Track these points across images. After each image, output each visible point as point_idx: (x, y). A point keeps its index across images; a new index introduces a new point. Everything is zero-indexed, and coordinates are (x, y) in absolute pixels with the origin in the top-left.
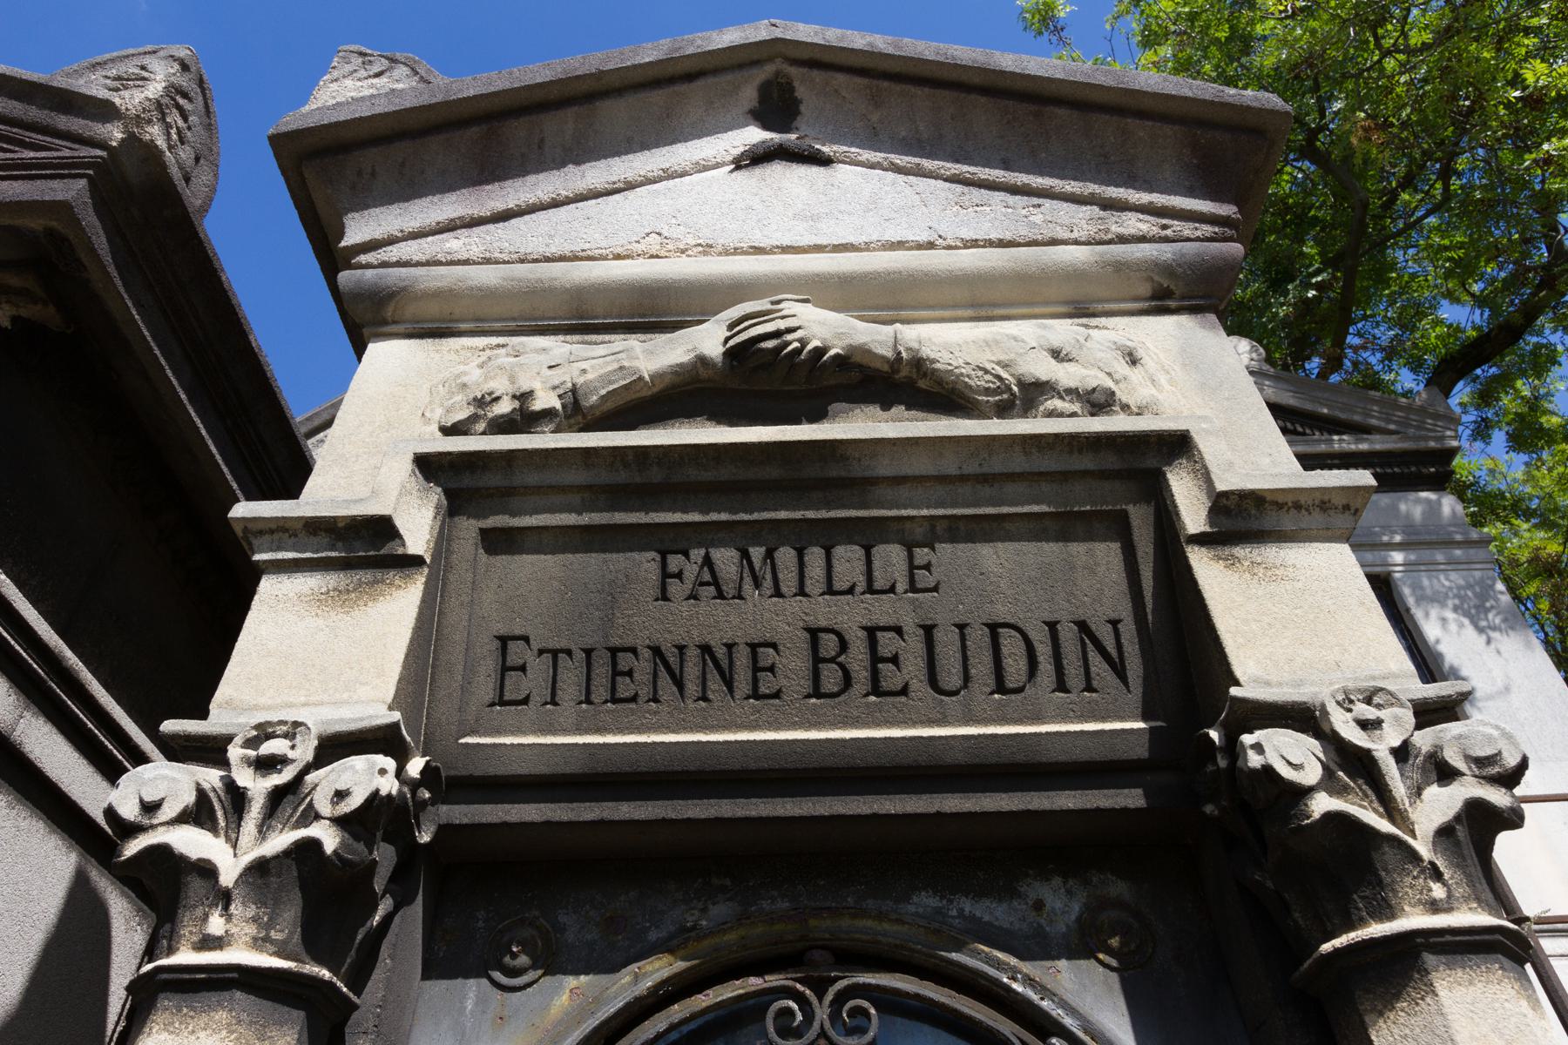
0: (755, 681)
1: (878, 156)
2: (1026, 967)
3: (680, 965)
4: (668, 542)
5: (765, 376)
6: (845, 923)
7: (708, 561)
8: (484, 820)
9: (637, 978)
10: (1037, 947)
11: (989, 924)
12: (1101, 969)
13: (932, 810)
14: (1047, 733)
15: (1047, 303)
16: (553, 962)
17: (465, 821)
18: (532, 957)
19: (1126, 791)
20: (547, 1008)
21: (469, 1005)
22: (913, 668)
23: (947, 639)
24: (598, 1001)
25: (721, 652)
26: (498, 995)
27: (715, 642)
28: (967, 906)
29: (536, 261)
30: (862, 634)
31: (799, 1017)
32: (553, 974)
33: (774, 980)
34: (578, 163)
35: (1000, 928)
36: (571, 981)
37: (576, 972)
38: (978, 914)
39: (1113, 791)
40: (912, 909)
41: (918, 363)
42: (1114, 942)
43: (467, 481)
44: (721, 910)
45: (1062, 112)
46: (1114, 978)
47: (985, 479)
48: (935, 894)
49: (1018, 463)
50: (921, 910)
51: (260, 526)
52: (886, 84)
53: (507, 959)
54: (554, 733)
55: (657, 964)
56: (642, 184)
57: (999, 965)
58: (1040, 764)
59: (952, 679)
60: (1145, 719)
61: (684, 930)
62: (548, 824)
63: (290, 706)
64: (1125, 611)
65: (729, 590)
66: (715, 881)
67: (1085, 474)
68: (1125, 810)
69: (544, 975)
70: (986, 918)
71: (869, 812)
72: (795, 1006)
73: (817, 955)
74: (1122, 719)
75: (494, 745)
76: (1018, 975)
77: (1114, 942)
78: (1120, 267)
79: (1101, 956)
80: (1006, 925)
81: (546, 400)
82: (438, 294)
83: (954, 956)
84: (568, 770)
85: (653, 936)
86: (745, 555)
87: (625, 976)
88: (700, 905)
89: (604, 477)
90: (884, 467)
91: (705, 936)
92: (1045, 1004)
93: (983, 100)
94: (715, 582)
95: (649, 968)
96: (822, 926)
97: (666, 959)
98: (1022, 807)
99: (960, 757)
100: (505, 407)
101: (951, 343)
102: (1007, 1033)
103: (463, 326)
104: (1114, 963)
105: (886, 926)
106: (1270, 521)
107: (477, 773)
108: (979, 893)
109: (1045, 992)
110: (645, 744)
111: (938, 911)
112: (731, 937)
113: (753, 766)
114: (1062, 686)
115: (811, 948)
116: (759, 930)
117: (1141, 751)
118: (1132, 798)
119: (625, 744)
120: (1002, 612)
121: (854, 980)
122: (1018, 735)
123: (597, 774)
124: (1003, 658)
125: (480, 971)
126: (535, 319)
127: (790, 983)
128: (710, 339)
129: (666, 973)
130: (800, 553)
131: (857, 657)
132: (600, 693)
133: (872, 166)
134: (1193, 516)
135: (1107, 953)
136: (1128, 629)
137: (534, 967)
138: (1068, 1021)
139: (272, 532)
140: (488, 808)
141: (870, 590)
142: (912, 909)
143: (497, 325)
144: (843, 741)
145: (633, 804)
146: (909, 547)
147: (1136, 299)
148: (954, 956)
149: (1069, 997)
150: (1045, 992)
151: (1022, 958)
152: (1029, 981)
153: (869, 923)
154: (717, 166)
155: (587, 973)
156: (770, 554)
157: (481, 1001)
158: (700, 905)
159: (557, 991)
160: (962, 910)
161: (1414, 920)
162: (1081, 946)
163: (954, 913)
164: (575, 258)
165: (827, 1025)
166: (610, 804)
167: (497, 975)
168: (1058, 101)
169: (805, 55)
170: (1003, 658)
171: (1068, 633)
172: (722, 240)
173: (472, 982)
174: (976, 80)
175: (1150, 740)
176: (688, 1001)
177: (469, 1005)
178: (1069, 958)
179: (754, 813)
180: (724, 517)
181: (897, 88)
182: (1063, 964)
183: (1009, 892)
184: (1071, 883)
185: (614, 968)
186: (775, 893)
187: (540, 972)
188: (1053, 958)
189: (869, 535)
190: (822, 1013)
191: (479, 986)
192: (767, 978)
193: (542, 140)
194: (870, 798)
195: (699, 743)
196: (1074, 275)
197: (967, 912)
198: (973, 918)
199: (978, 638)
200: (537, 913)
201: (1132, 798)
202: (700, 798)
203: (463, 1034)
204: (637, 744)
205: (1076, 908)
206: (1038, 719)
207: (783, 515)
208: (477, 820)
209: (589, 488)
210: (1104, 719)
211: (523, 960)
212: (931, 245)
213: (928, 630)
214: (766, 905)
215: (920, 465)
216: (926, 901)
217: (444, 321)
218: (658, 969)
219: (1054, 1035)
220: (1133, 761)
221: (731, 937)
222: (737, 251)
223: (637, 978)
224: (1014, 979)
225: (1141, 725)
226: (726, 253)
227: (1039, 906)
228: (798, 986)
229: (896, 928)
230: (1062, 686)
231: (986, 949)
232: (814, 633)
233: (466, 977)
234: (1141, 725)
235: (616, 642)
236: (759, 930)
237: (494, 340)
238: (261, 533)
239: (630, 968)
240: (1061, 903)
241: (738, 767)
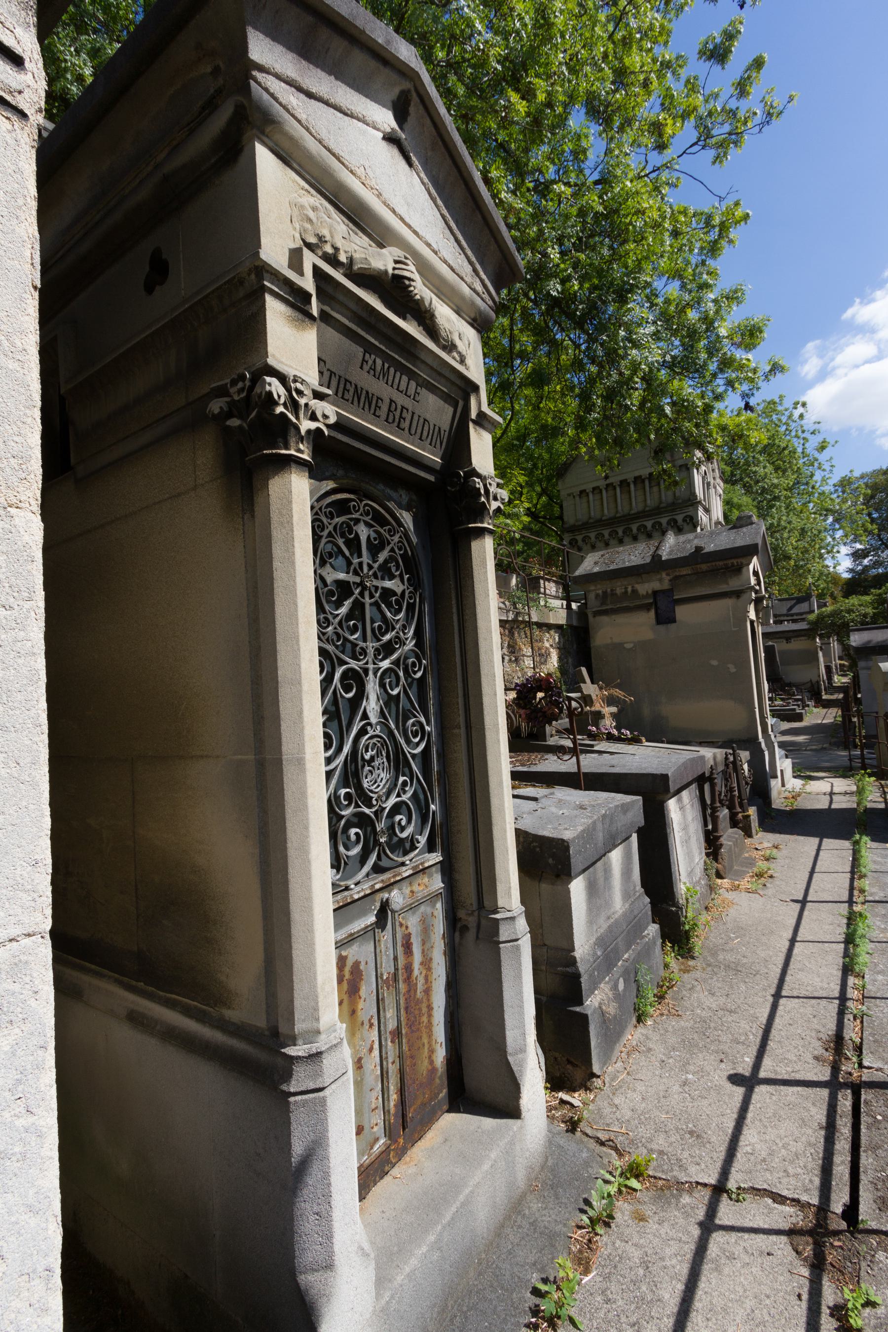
0: (375, 410)
1: (426, 180)
4: (369, 349)
5: (394, 289)
7: (374, 362)
15: (453, 303)
22: (405, 425)
23: (416, 418)
25: (370, 396)
27: (417, 413)
29: (325, 147)
30: (388, 401)
34: (337, 78)
41: (432, 316)
45: (479, 216)
47: (440, 374)
49: (447, 373)
51: (268, 268)
52: (440, 143)
56: (358, 119)
59: (413, 432)
63: (307, 375)
64: (447, 430)
65: (377, 374)
67: (457, 385)
78: (473, 304)
81: (343, 258)
82: (291, 138)
85: (327, 474)
86: (383, 365)
89: (364, 315)
90: (423, 356)
93: (463, 186)
94: (374, 370)
99: (409, 454)
100: (329, 249)
101: (444, 314)
103: (295, 165)
106: (486, 424)
114: (430, 444)
117: (438, 468)
120: (428, 417)
124: (420, 428)
126: (320, 185)
128: (383, 260)
130: (395, 371)
131: (385, 408)
132: (340, 394)
133: (423, 183)
134: (473, 415)
136: (447, 434)
139: (272, 274)
141: (406, 394)
143: (308, 177)
146: (417, 385)
147: (470, 317)
154: (378, 129)
156: (388, 368)
161: (485, 525)
164: (338, 158)
168: (497, 241)
169: (422, 92)
170: (420, 428)
171: (437, 429)
172: (385, 195)
174: (465, 174)
180: (384, 348)
181: (443, 150)
183: (396, 491)
189: (412, 375)
193: (328, 49)
196: (462, 297)
199: (422, 420)
201: (432, 478)
206: (424, 450)
207: (397, 357)
209: (355, 313)
212: (436, 253)
213: (413, 413)
215: (429, 361)
217: (287, 154)
222: (388, 206)
226: (385, 203)
230: (430, 444)
232: (391, 401)
235: (347, 377)
237: (307, 186)
238: (267, 271)
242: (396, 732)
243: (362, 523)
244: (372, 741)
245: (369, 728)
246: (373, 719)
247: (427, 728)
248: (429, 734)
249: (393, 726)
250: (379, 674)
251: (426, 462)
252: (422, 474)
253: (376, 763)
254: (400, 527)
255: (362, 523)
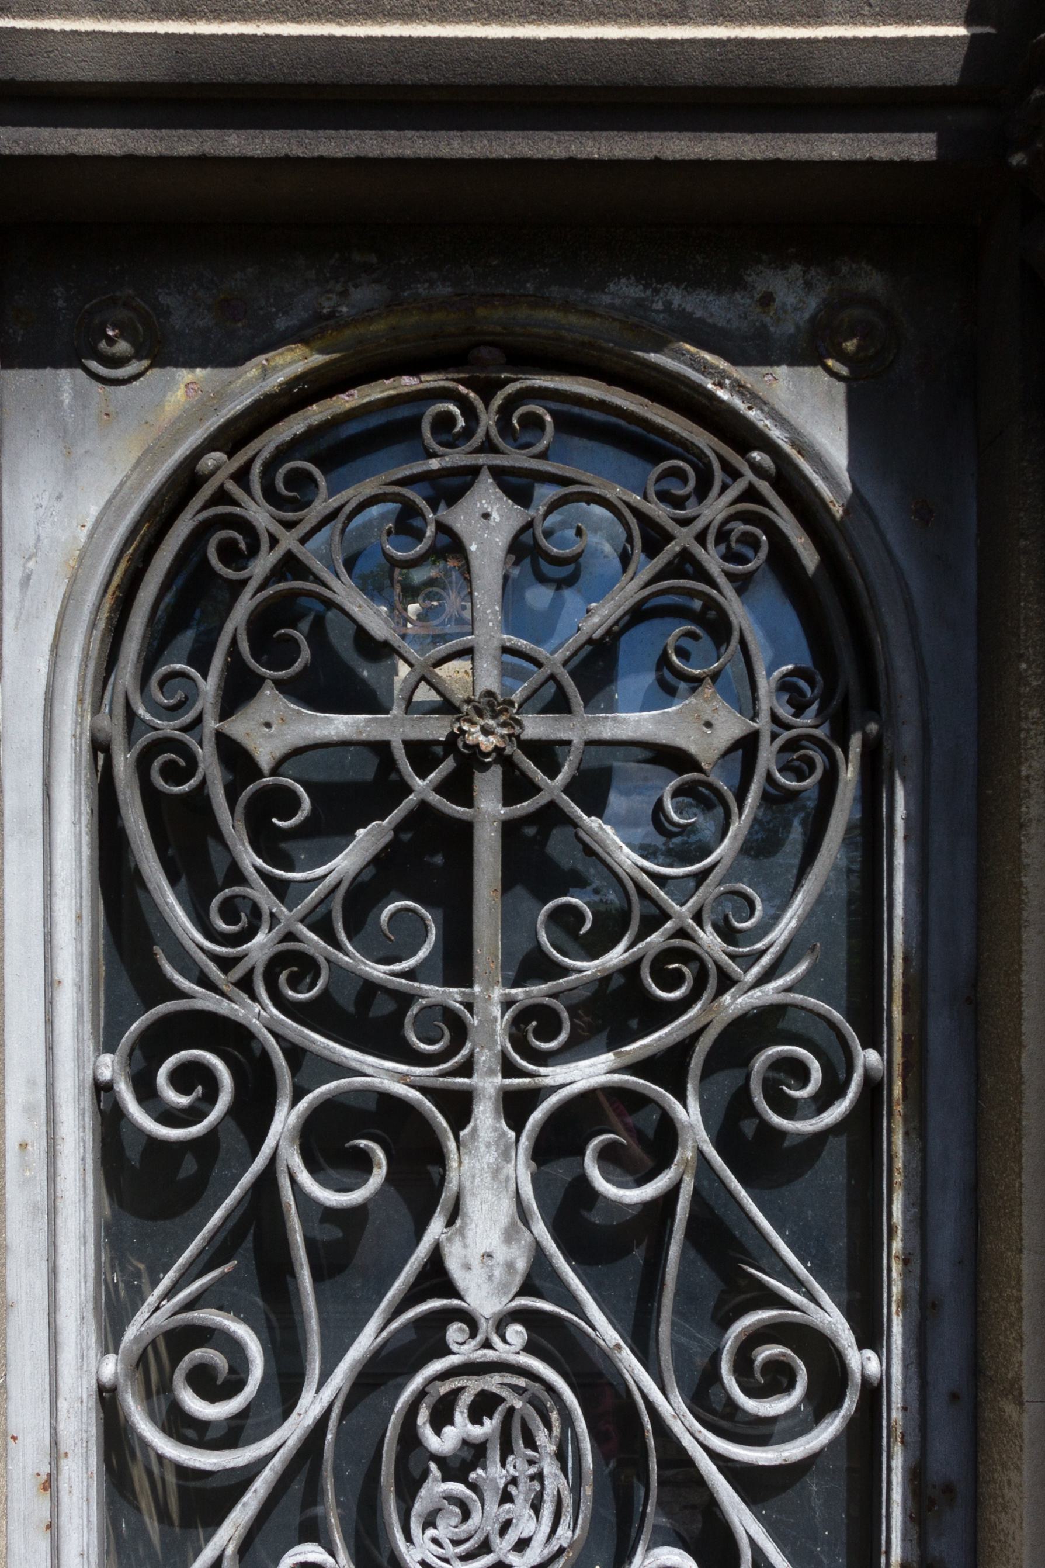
2: (738, 373)
3: (318, 359)
6: (522, 313)
8: (43, 151)
9: (265, 373)
10: (755, 349)
11: (701, 320)
12: (827, 378)
13: (648, 155)
14: (826, 40)
16: (162, 351)
17: (18, 151)
18: (132, 343)
19: (915, 136)
20: (160, 405)
21: (66, 398)
24: (221, 396)
26: (99, 388)
28: (676, 297)
31: (461, 423)
32: (162, 365)
33: (431, 381)
35: (714, 326)
36: (185, 375)
37: (191, 365)
38: (689, 308)
39: (897, 136)
40: (606, 299)
42: (850, 346)
43: (325, 443)
44: (365, 294)
46: (841, 388)
48: (638, 281)
50: (617, 302)
53: (103, 345)
54: (122, 16)
55: (289, 357)
57: (705, 369)
58: (807, 90)
60: (968, 23)
61: (319, 317)
62: (130, 159)
66: (357, 257)
68: (906, 164)
69: (151, 366)
70: (699, 314)
71: (564, 155)
72: (456, 411)
73: (484, 352)
74: (936, 20)
75: (37, 32)
76: (723, 381)
77: (850, 346)
79: (830, 362)
80: (721, 323)
83: (653, 357)
84: (148, 77)
85: (281, 324)
87: (251, 370)
88: (339, 287)
91: (347, 325)
92: (753, 414)
95: (280, 361)
96: (493, 317)
97: (299, 350)
98: (770, 155)
99: (695, 74)
102: (702, 445)
104: (844, 371)
105: (573, 319)
107: (21, 77)
108: (694, 282)
109: (755, 399)
110: (254, 38)
111: (639, 303)
112: (379, 327)
113: (408, 79)
115: (478, 344)
116: (413, 319)
117: (949, 74)
118: (919, 146)
119: (225, 37)
121: (529, 383)
122: (784, 41)
123: (190, 85)
125: (72, 360)
127: (451, 384)
129: (299, 368)
135: (838, 359)
137: (138, 356)
138: (776, 434)
140: (45, 132)
142: (606, 299)
144: (535, 42)
145: (244, 134)
148: (653, 357)
149: (781, 407)
150: (755, 399)
151: (735, 362)
152: (739, 388)
153: (552, 314)
155: (203, 366)
157: (78, 394)
158: (339, 287)
159: (169, 386)
160: (670, 303)
162: (806, 351)
163: (659, 306)
165: (494, 432)
166: (212, 133)
167: (94, 365)
173: (63, 372)
175: (967, 56)
176: (328, 403)
177: (66, 398)
178: (791, 364)
179: (408, 153)
182: (782, 371)
183: (732, 282)
184: (813, 272)
185: (237, 361)
186: (434, 275)
187: (146, 363)
188: (772, 364)
190: (488, 420)
191: (73, 377)
192: (423, 377)
194: (566, 135)
195: (331, 38)
197: (675, 306)
198: (682, 314)
200: (131, 292)
201: (919, 146)
202: (336, 128)
203: (65, 431)
204: (241, 37)
205: (813, 303)
208: (33, 149)
210: (909, 20)
211: (122, 347)
214: (422, 289)
216: (626, 290)
218: (290, 363)
219: (755, 448)
220: (936, 88)
221: (379, 327)
223: (265, 373)
224: (721, 385)
225: (961, 31)
227: (767, 300)
228: (461, 388)
229: (585, 321)
231: (693, 349)
233: (57, 365)
234: (961, 31)
236: (413, 319)
239: (255, 361)
240: (794, 296)
241: (385, 79)
242: (629, 1362)
243: (486, 481)
244: (473, 1385)
245: (455, 1333)
246: (483, 1294)
247: (864, 1363)
248: (873, 1394)
249: (607, 1333)
250: (280, 1060)
251: (832, 75)
252: (832, 147)
253: (493, 1473)
254: (743, 450)
255: (486, 481)
